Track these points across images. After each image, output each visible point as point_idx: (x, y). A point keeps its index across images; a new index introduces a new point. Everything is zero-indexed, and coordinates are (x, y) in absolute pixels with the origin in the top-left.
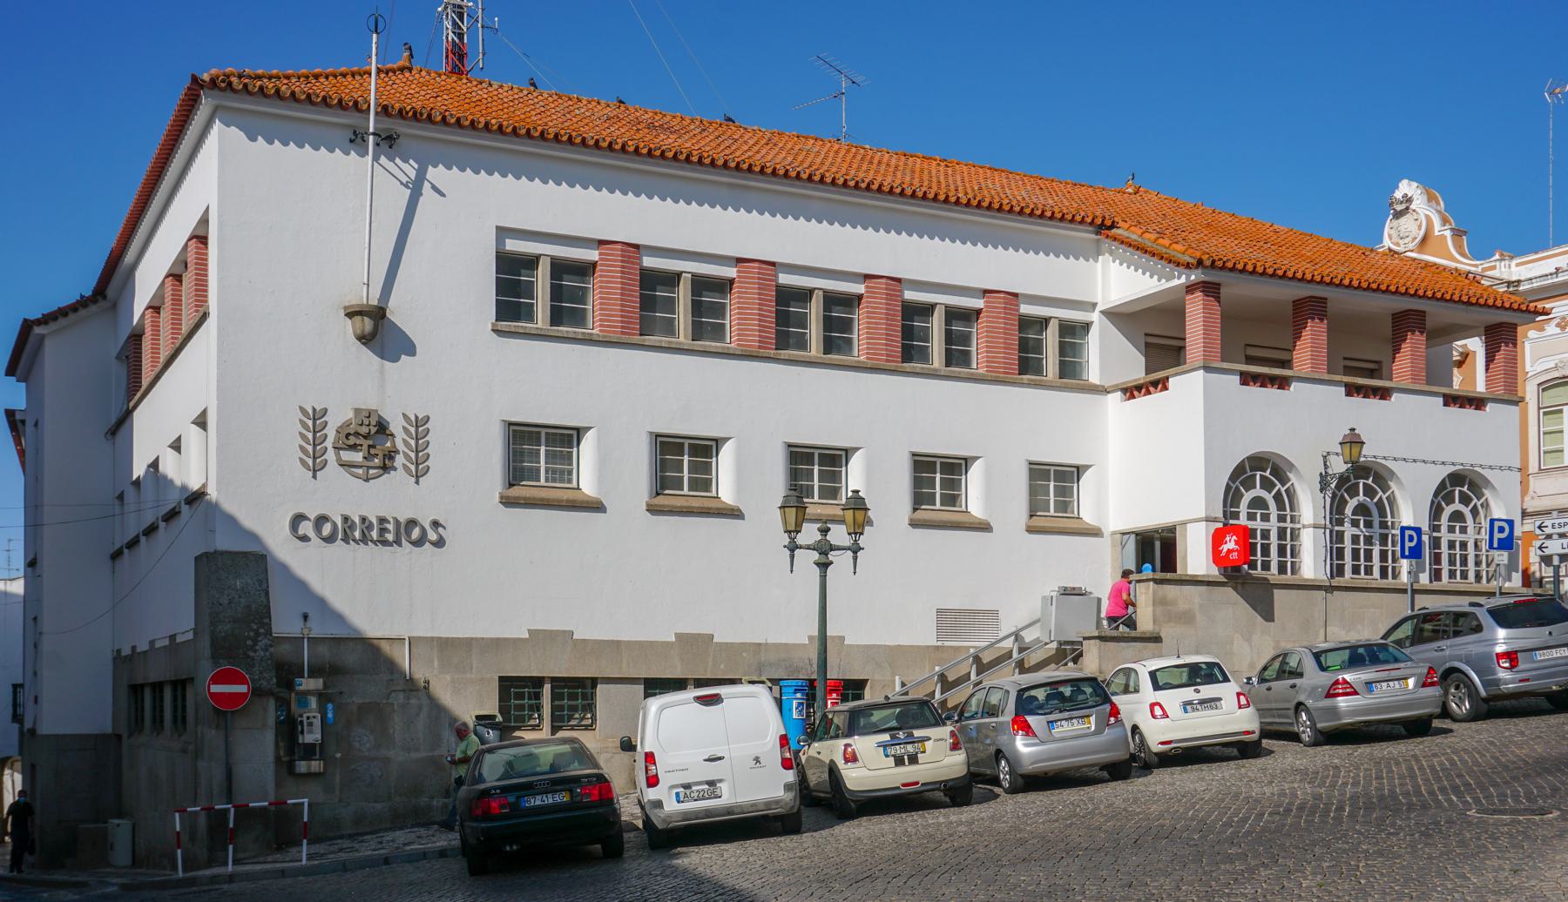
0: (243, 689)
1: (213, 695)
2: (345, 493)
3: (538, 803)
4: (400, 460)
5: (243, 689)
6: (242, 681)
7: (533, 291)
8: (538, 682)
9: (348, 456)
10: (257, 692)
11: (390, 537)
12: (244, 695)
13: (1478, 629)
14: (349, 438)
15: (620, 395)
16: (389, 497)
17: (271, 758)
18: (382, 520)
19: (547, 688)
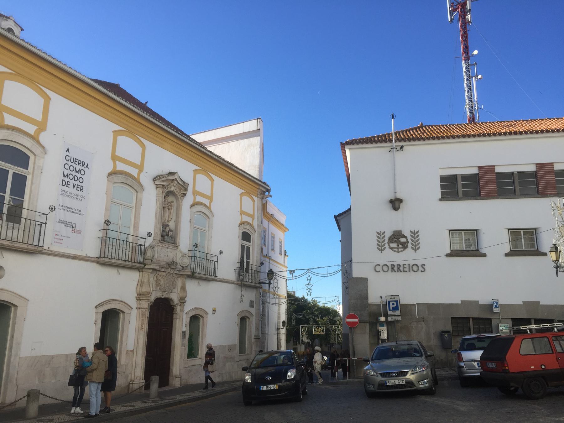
0: (356, 320)
1: (347, 322)
2: (391, 256)
3: (272, 388)
4: (410, 245)
5: (356, 320)
6: (356, 318)
7: (456, 187)
8: (469, 318)
9: (392, 245)
10: (361, 322)
11: (407, 269)
12: (356, 323)
13: (294, 345)
14: (391, 240)
15: (494, 218)
16: (407, 256)
17: (368, 343)
18: (392, 265)
19: (471, 320)
